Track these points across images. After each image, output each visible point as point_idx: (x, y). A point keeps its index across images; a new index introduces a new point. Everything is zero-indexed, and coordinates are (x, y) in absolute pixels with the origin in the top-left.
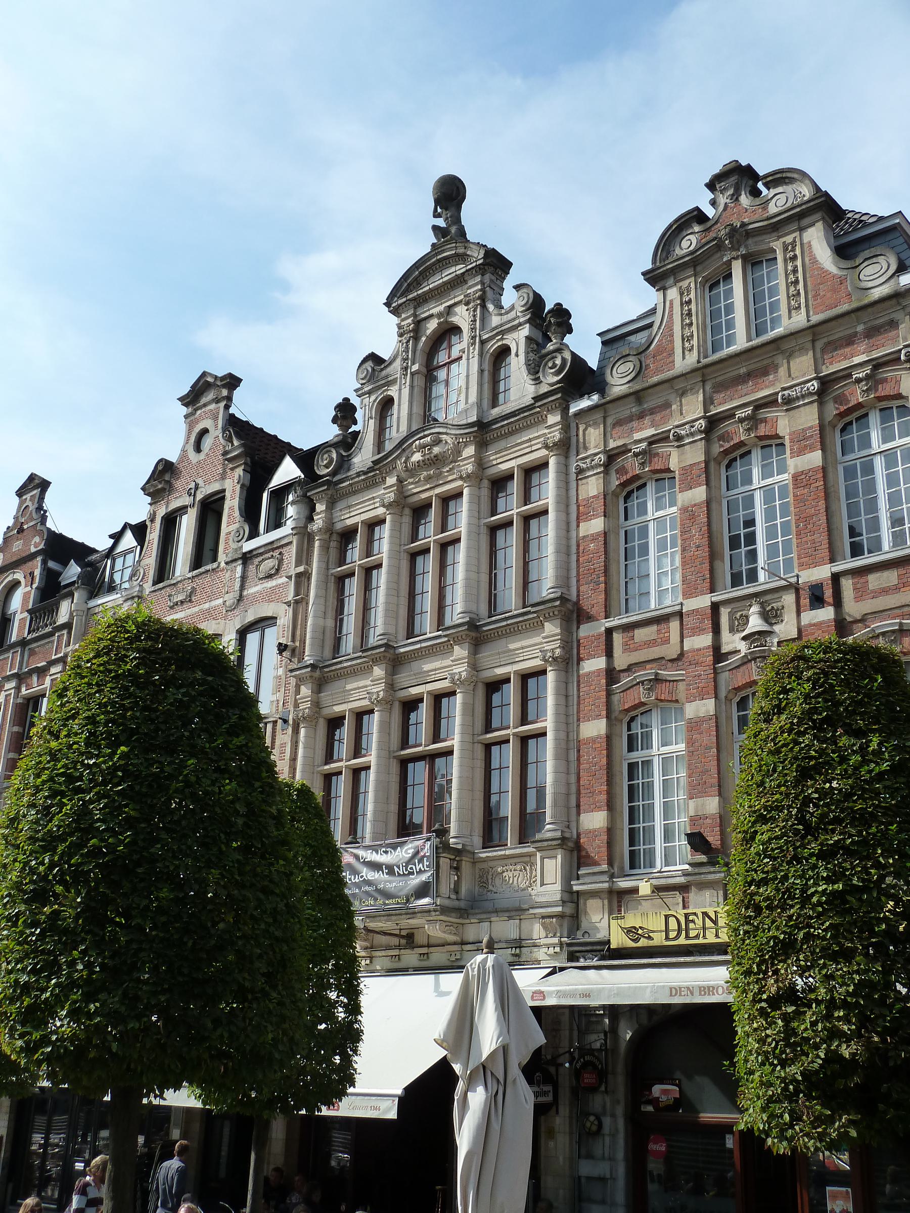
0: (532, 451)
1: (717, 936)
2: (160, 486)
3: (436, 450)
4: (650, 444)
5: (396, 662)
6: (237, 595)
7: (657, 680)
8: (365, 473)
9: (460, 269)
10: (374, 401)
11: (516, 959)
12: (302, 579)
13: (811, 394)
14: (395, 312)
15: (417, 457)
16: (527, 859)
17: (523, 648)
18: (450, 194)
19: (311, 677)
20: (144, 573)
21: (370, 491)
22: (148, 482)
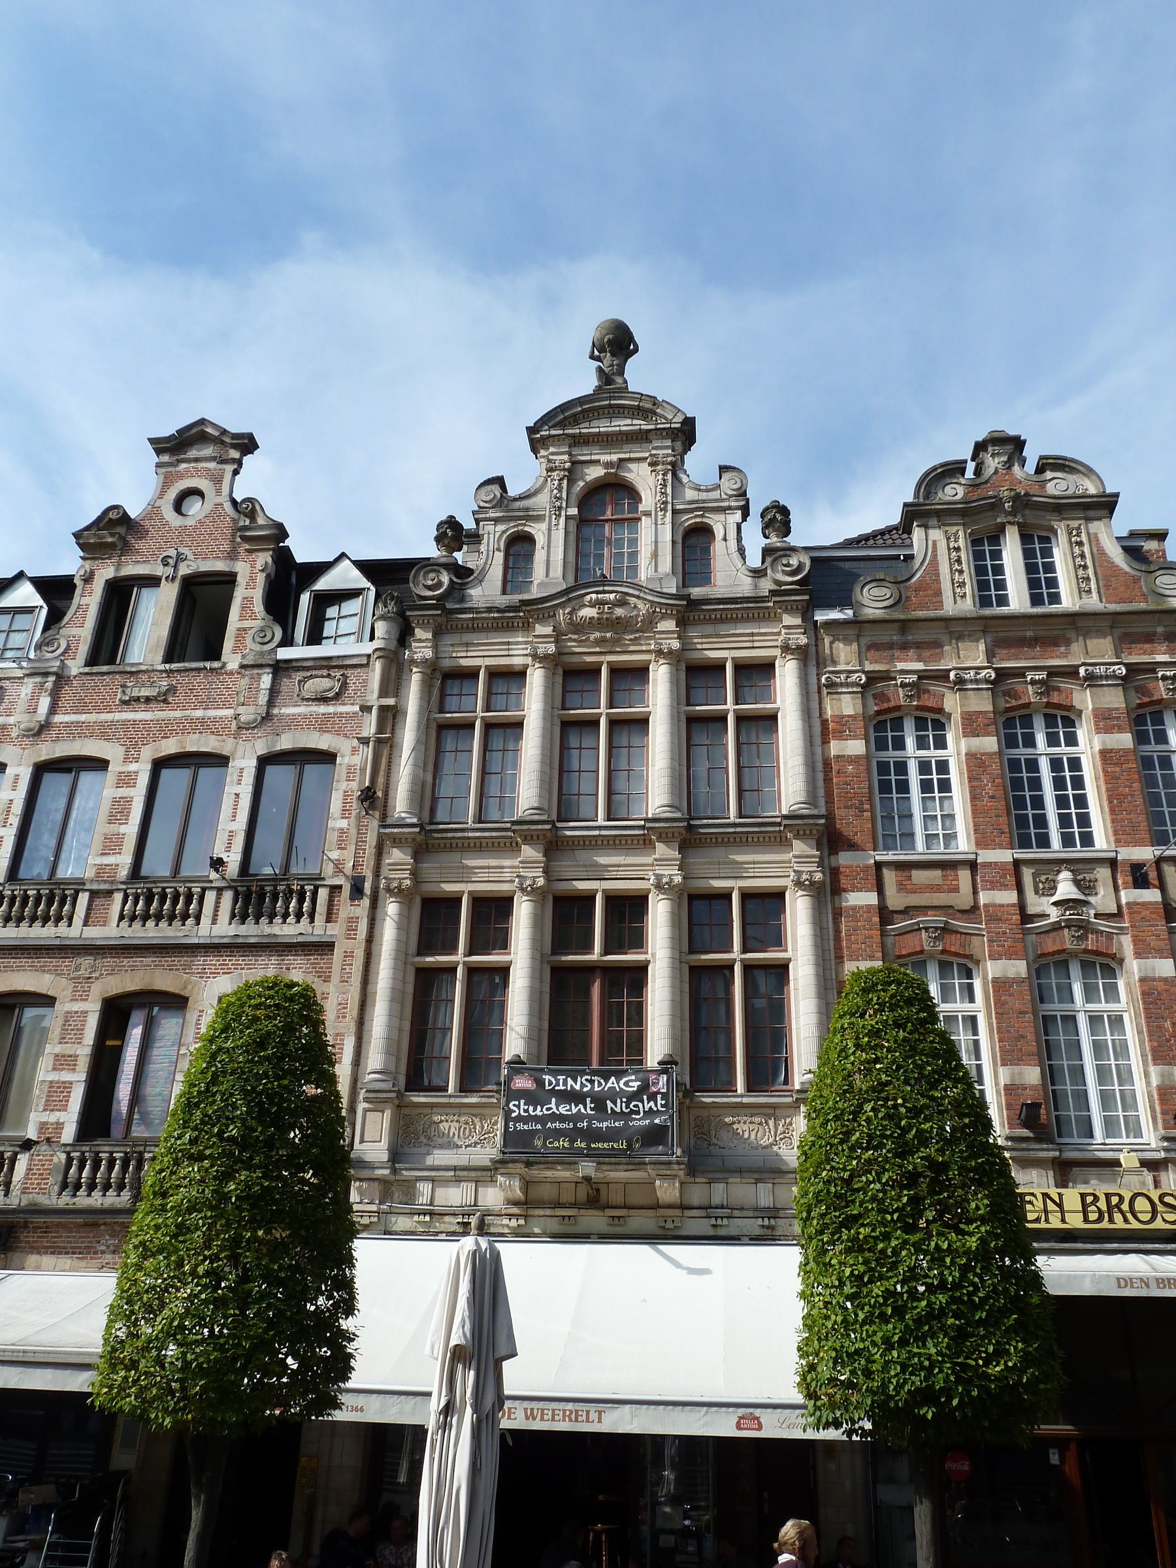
0: (753, 647)
1: (1063, 1221)
2: (110, 540)
3: (619, 612)
4: (920, 678)
5: (555, 846)
6: (263, 711)
7: (946, 930)
8: (499, 610)
9: (640, 424)
10: (504, 532)
11: (768, 1232)
12: (390, 717)
13: (1115, 677)
14: (536, 445)
15: (588, 612)
16: (771, 1111)
17: (754, 863)
18: (618, 343)
19: (414, 840)
20: (68, 648)
21: (507, 634)
22: (87, 528)
